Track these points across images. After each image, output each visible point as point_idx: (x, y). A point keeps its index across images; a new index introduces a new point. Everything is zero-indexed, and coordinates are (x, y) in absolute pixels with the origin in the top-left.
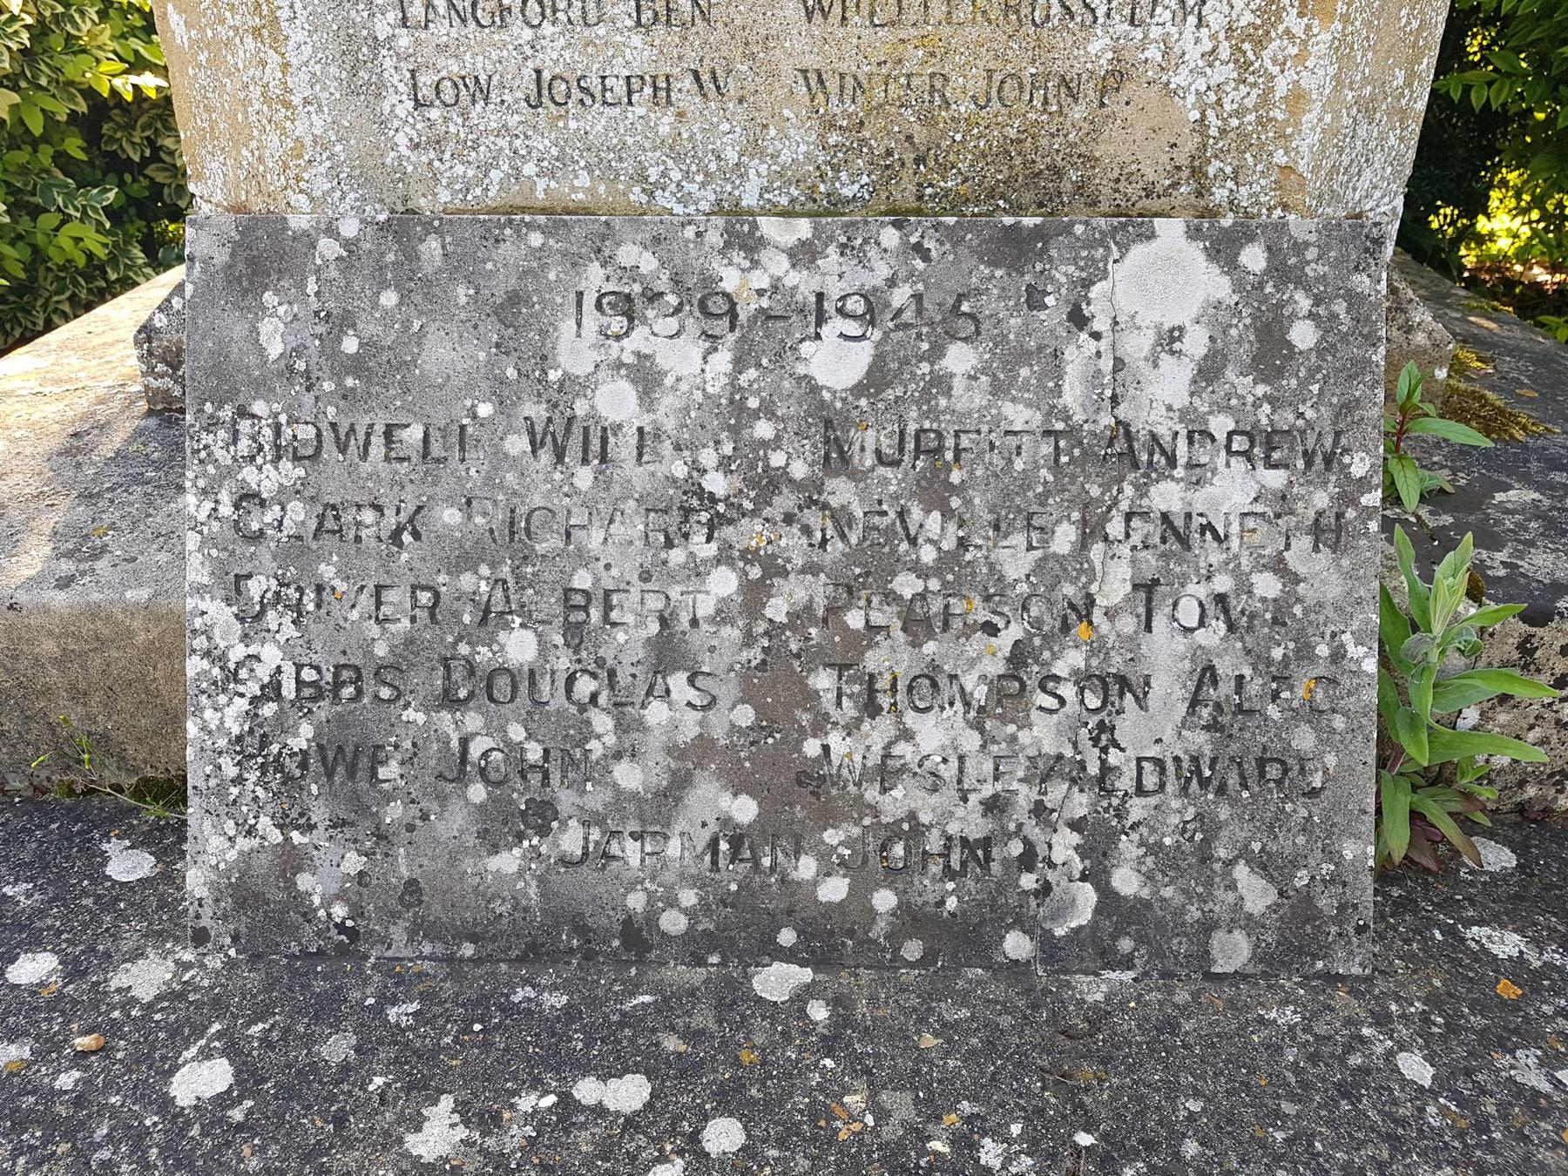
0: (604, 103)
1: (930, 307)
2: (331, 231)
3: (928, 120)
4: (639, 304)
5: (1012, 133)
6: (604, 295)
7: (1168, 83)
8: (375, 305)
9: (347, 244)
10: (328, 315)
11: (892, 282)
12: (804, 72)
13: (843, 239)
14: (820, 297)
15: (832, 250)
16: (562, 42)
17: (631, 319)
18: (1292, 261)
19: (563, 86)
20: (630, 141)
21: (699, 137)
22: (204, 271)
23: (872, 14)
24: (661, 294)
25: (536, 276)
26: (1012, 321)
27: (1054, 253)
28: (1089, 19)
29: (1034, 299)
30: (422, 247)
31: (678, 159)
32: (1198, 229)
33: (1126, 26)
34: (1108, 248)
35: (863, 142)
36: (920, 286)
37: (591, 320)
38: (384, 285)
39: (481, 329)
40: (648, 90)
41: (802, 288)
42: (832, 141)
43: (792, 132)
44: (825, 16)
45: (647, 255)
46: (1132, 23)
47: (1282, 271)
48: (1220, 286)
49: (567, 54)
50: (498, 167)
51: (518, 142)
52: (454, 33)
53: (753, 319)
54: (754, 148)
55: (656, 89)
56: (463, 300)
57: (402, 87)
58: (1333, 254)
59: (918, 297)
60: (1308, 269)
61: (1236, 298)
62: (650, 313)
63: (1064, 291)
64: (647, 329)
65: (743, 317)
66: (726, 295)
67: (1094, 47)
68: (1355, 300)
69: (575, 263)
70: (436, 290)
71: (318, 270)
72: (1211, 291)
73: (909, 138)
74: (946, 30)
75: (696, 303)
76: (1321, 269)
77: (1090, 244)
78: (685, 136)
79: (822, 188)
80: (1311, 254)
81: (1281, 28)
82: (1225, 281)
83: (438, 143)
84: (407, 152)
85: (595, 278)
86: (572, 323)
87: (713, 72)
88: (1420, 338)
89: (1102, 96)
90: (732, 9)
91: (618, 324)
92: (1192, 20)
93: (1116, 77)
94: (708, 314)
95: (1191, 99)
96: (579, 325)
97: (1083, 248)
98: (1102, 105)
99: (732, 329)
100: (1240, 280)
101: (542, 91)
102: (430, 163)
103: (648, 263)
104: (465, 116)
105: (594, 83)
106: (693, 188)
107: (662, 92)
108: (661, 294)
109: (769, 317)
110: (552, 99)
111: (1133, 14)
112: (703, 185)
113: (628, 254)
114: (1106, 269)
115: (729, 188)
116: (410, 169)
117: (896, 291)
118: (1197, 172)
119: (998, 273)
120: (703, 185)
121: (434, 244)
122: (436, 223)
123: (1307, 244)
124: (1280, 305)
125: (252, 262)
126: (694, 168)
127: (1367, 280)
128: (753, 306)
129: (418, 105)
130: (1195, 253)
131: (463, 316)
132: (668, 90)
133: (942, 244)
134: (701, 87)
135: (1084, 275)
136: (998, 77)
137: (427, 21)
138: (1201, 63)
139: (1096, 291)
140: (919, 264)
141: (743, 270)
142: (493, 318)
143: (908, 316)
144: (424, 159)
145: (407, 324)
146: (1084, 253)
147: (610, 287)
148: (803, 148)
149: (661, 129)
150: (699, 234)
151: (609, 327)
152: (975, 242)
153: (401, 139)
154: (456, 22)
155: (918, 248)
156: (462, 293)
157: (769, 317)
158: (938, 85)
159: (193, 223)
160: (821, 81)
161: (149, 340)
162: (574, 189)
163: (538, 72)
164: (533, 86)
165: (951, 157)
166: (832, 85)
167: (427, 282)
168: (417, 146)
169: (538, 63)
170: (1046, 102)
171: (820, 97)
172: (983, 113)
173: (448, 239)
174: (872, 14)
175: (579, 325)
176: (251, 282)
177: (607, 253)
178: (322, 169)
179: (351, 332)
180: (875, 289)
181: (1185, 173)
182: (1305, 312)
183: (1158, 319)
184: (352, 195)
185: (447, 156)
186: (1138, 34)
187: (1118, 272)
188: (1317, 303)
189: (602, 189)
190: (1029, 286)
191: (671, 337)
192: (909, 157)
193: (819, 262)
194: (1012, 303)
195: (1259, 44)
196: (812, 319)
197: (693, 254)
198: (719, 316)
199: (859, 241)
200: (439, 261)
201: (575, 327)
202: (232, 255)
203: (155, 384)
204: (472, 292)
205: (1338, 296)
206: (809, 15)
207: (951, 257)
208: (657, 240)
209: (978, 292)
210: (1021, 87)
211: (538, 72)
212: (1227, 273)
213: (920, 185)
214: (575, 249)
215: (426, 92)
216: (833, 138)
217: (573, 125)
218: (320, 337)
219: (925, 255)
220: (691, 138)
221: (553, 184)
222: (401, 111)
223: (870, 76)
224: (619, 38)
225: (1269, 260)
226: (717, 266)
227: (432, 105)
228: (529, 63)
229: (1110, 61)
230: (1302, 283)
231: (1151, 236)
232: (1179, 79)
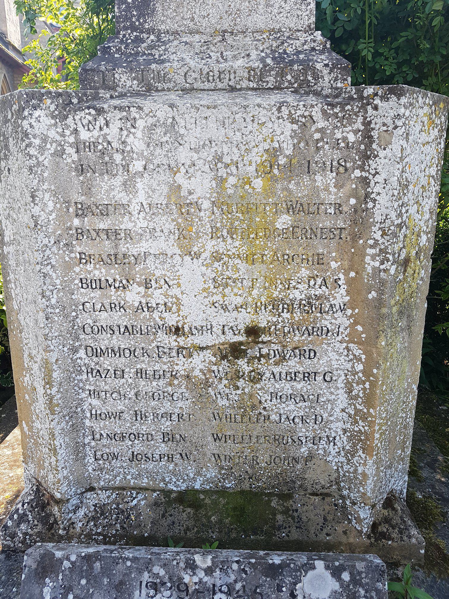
0: (153, 461)
1: (247, 590)
2: (68, 559)
3: (252, 467)
4: (159, 586)
5: (279, 471)
6: (148, 583)
7: (326, 459)
8: (79, 584)
9: (73, 563)
10: (65, 586)
11: (236, 581)
12: (214, 454)
13: (221, 566)
14: (214, 585)
15: (218, 570)
16: (140, 445)
17: (156, 591)
18: (358, 578)
19: (140, 456)
20: (160, 471)
21: (182, 470)
22: (28, 570)
23: (234, 440)
24: (166, 583)
25: (128, 575)
26: (273, 596)
27: (285, 573)
28: (300, 443)
29: (279, 589)
30: (95, 565)
31: (175, 476)
32: (328, 566)
33: (312, 445)
34: (301, 572)
35: (233, 473)
36: (244, 583)
37: (144, 592)
38: (82, 577)
39: (111, 593)
40: (166, 458)
41: (208, 582)
42: (222, 472)
43: (210, 470)
44: (220, 440)
45: (162, 570)
46: (314, 444)
47: (355, 581)
48: (336, 586)
49: (142, 448)
50: (119, 476)
51: (126, 470)
52: (108, 442)
53: (193, 593)
54: (198, 473)
55: (168, 457)
56: (106, 583)
57: (91, 455)
58: (370, 576)
59: (244, 587)
60: (363, 581)
61: (341, 590)
62: (162, 589)
63: (288, 586)
64: (161, 594)
65: (190, 591)
66: (185, 584)
67: (302, 450)
68: (378, 591)
69: (140, 572)
70: (98, 579)
71: (63, 571)
72: (333, 587)
73: (247, 472)
74: (257, 445)
75: (176, 586)
76: (367, 581)
77: (296, 571)
78: (177, 470)
79: (220, 484)
80: (363, 575)
81: (358, 454)
82: (338, 584)
83: (101, 470)
84: (92, 472)
85: (146, 577)
86: (138, 592)
87: (186, 453)
88: (414, 540)
89: (306, 462)
90: (192, 438)
91: (152, 592)
92: (332, 444)
93: (310, 457)
94: (179, 590)
95: (334, 464)
96: (140, 592)
97: (294, 572)
98: (306, 465)
99: (187, 595)
100: (342, 583)
101: (134, 457)
102: (99, 474)
103: (162, 572)
104: (110, 463)
105: (150, 455)
106: (180, 483)
107: (170, 458)
108: (166, 583)
109: (198, 592)
110: (137, 459)
111: (314, 442)
112: (183, 483)
113: (156, 569)
114: (301, 579)
115: (191, 484)
116: (92, 476)
117: (237, 584)
118: (338, 483)
119: (268, 579)
120: (183, 483)
121: (98, 564)
122: (99, 557)
123: (362, 572)
124: (355, 593)
125: (43, 568)
126: (180, 478)
127: (381, 585)
128: (193, 588)
129: (96, 459)
130: (328, 574)
131: (105, 588)
132: (172, 458)
133: (251, 569)
134: (182, 457)
135: (294, 581)
136: (273, 457)
137: (100, 439)
138: (336, 454)
139: (298, 586)
140: (244, 576)
141: (191, 576)
142: (114, 589)
143: (241, 593)
144: (97, 473)
145: (88, 591)
146: (294, 574)
147: (150, 580)
148: (214, 474)
149: (170, 468)
150: (177, 563)
151: (149, 593)
152: (261, 569)
153: (90, 469)
154: (109, 439)
155: (243, 570)
156: (106, 581)
157: (198, 592)
158: (255, 458)
159: (27, 554)
160: (219, 456)
161: (6, 530)
162: (142, 483)
163: (133, 452)
164: (131, 456)
165: (260, 477)
166: (223, 458)
167: (95, 577)
168: (95, 470)
169: (133, 450)
170: (289, 464)
171: (219, 461)
172: (269, 466)
173: (103, 563)
174: (234, 440)
175: (140, 592)
176: (42, 575)
177: (150, 569)
178: (65, 485)
179: (71, 593)
180: (231, 583)
181: (334, 483)
182: (363, 595)
183: (317, 596)
184: (74, 489)
185: (104, 473)
186: (316, 447)
187: (305, 580)
188: (366, 592)
189: (151, 483)
190: (278, 584)
191: (168, 598)
192: (247, 477)
193: (214, 574)
194: (272, 590)
195: (353, 456)
196: (211, 593)
197: (176, 570)
198: (183, 591)
199: (226, 567)
200: (99, 570)
201: (139, 593)
202: (38, 565)
203: (5, 543)
204: (108, 580)
205: (373, 590)
206: (215, 440)
207: (253, 574)
208: (165, 565)
209: (262, 585)
210: (281, 460)
211: (133, 452)
212: (338, 581)
213: (250, 484)
214: (140, 567)
215: (98, 456)
216: (223, 472)
217: (143, 466)
218: (61, 594)
219: (246, 573)
220: (179, 470)
221: (136, 481)
222: (90, 461)
223: (234, 456)
224: (157, 444)
225: (350, 577)
226: (183, 574)
227: (100, 460)
228: (131, 450)
229: (308, 454)
230: (361, 585)
231: (314, 568)
232: (330, 458)
